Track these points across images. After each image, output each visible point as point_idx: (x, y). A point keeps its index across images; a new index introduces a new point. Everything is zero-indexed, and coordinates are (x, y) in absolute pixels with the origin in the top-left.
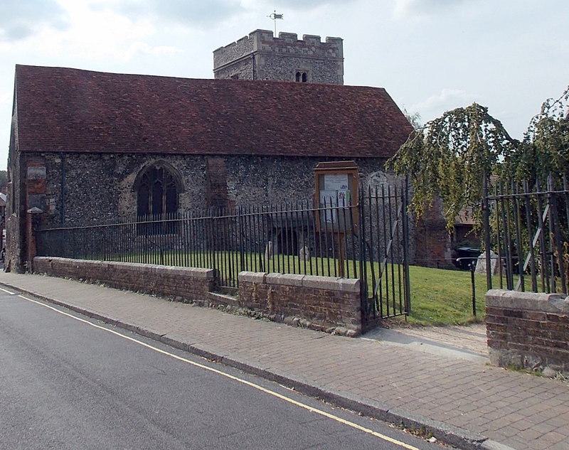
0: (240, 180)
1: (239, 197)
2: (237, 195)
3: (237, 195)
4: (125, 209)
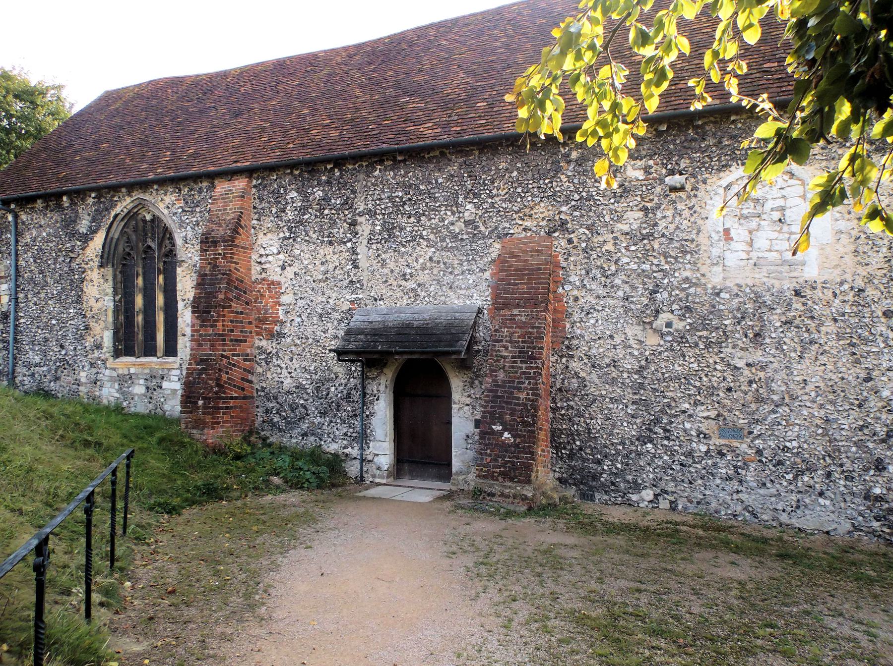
0: (290, 229)
1: (289, 272)
2: (283, 268)
3: (283, 268)
4: (92, 302)
